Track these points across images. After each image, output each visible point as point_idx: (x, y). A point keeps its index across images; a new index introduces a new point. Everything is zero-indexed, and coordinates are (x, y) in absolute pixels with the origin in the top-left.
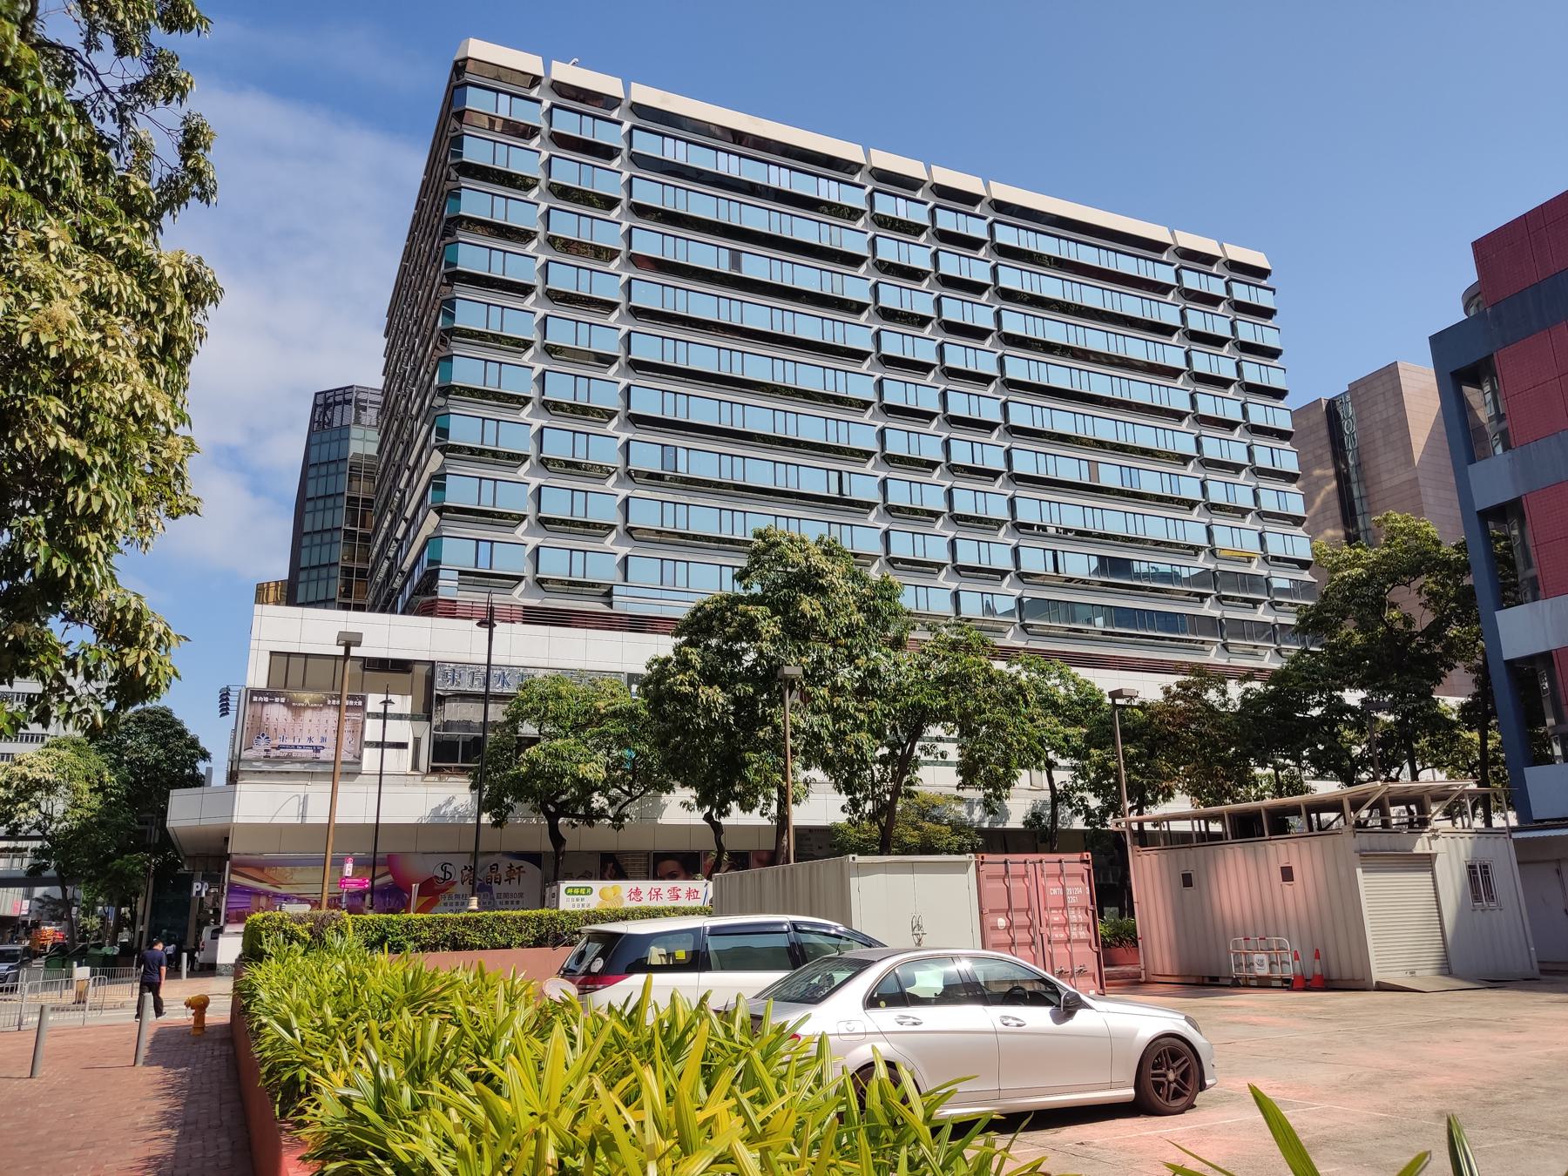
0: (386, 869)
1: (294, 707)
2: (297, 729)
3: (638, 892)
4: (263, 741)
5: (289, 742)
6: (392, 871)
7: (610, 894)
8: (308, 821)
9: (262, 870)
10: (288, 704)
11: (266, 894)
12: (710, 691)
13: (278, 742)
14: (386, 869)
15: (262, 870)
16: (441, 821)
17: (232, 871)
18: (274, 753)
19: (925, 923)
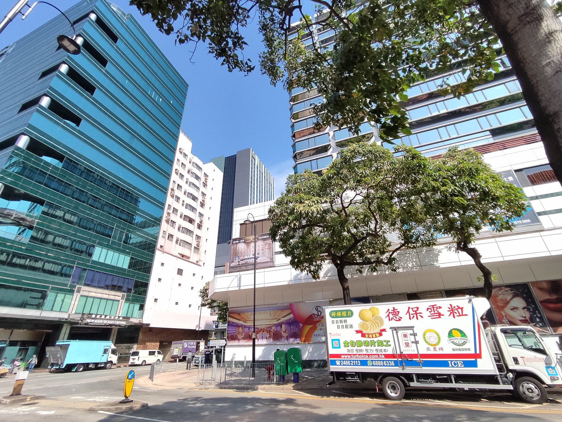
0: (290, 311)
1: (247, 243)
2: (249, 251)
3: (395, 312)
4: (237, 258)
5: (246, 257)
6: (292, 312)
7: (369, 315)
8: (242, 288)
9: (239, 314)
10: (245, 242)
11: (242, 326)
12: (397, 142)
13: (242, 258)
14: (290, 311)
15: (239, 314)
16: (297, 282)
17: (229, 316)
18: (241, 262)
19: (273, 86)
